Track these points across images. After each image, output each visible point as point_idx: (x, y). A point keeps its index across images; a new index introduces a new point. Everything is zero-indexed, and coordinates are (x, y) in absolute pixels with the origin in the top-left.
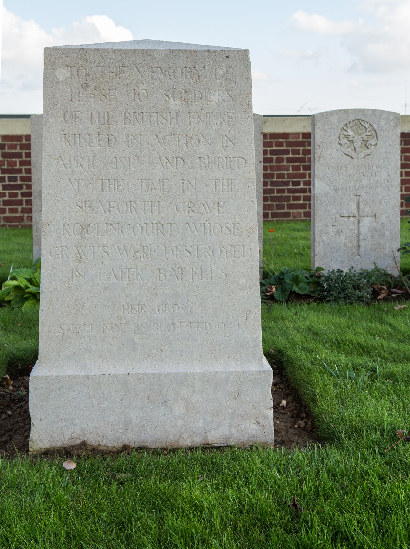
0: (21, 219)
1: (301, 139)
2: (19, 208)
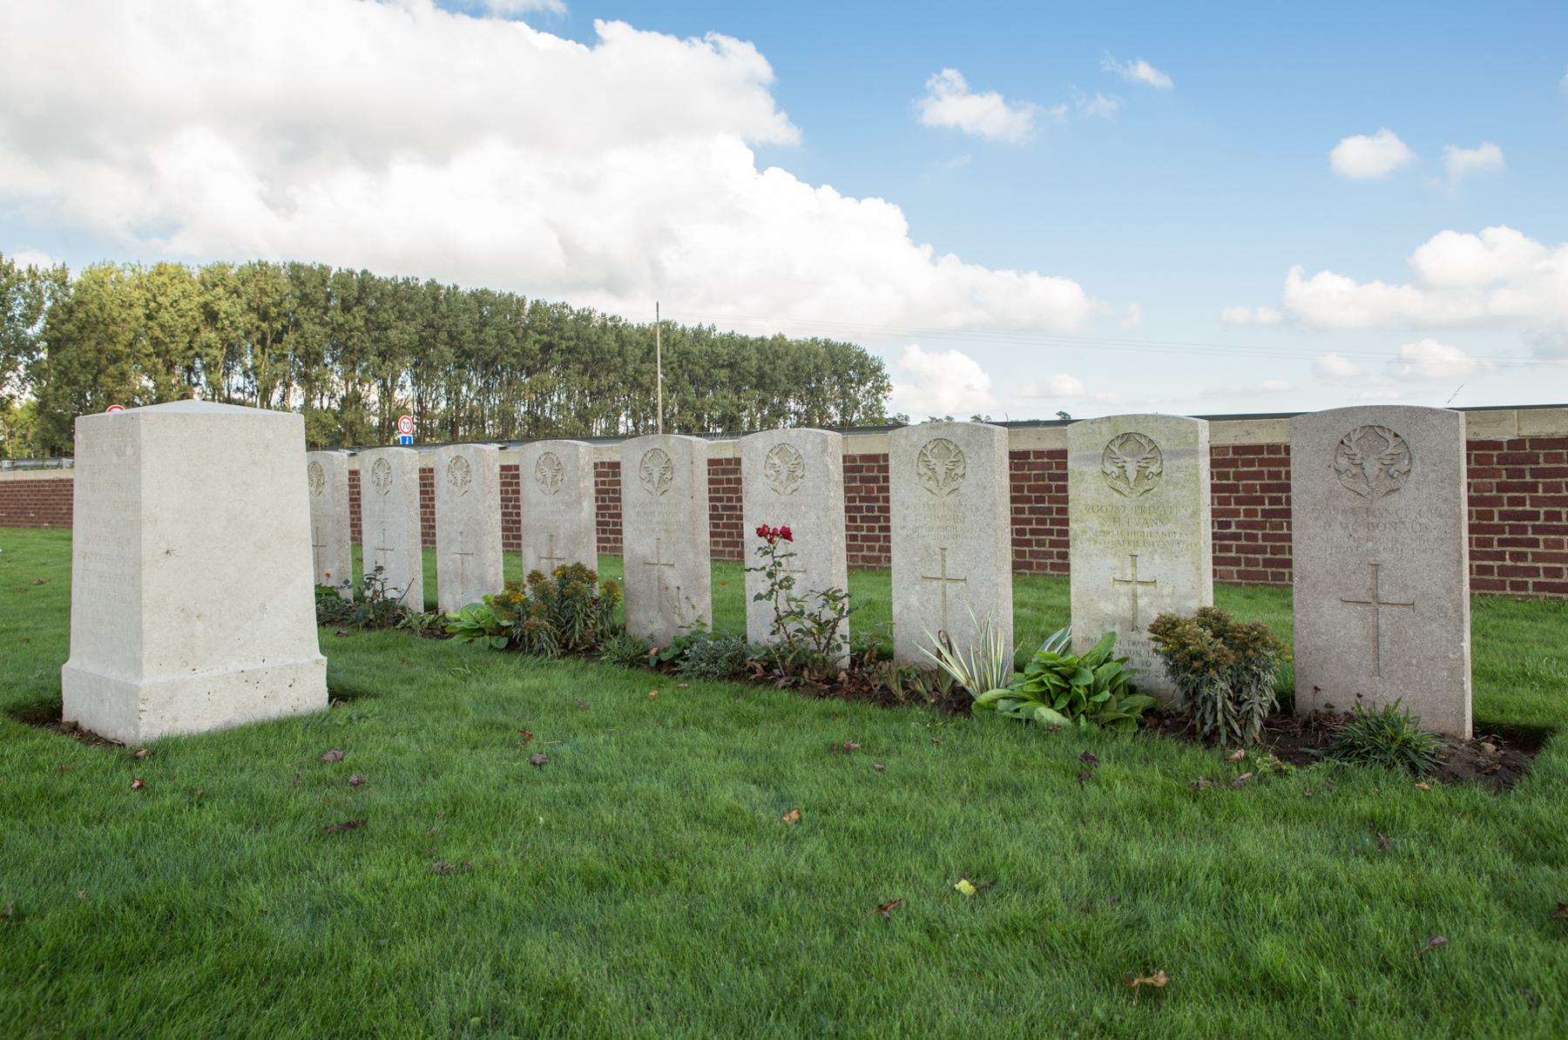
0: (878, 559)
1: (1231, 456)
2: (877, 545)
